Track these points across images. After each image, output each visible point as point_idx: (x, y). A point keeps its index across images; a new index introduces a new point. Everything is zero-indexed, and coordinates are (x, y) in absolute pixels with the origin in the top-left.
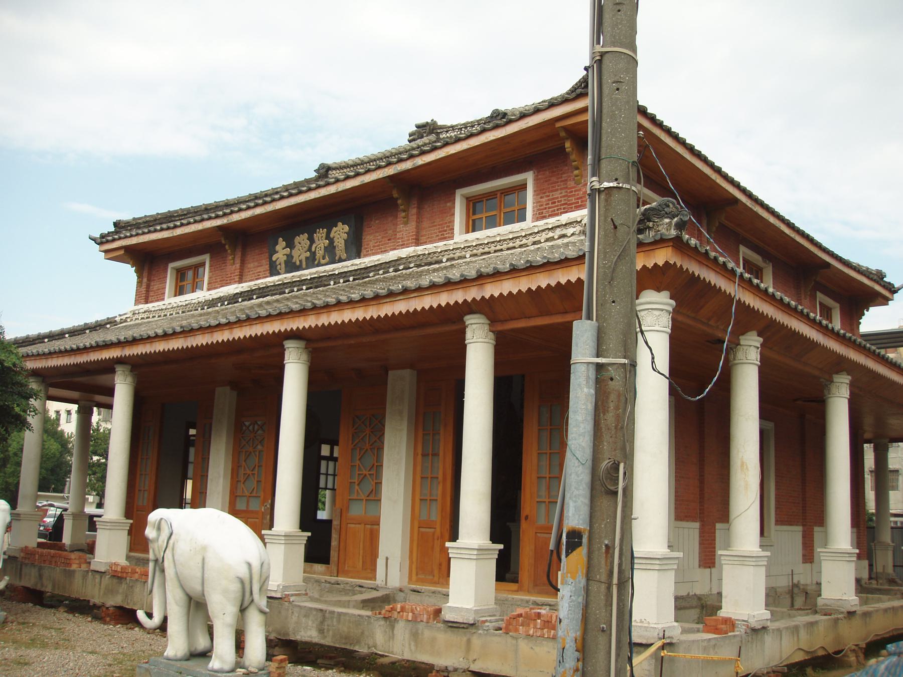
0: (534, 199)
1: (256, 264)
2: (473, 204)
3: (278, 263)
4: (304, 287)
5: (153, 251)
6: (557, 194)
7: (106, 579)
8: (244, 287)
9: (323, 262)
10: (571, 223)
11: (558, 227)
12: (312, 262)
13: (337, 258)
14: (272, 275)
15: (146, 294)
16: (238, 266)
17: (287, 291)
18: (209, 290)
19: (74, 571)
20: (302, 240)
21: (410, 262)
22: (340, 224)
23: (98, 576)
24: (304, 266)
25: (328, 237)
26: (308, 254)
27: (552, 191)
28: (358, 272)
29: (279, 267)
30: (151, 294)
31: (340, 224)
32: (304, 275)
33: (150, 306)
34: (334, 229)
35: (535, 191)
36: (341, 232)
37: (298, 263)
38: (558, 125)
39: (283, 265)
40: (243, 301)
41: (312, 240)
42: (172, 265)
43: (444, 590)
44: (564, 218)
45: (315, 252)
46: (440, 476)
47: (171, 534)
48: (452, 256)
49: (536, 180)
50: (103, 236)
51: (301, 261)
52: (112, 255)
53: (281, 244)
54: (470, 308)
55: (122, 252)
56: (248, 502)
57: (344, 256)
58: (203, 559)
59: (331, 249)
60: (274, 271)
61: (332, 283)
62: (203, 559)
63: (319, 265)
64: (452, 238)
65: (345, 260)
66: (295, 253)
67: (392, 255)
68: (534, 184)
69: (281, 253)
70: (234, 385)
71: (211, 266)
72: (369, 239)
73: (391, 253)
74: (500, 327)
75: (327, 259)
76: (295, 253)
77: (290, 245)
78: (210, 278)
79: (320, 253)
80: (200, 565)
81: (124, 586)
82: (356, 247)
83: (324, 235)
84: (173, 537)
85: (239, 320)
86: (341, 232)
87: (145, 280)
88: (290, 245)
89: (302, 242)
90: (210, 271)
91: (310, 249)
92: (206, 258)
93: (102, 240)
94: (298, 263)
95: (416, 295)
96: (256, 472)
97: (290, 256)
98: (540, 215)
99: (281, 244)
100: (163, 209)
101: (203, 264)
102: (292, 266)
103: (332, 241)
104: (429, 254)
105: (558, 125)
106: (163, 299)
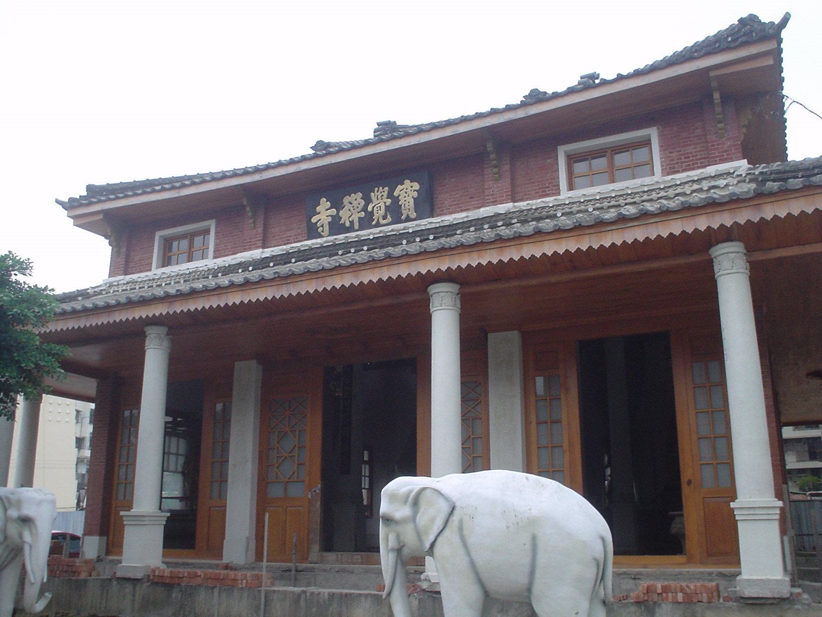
0: (661, 154)
1: (284, 228)
2: (572, 159)
3: (319, 224)
4: (365, 248)
5: (131, 219)
6: (690, 149)
7: (142, 590)
8: (268, 252)
9: (382, 222)
10: (720, 175)
11: (704, 179)
12: (367, 221)
13: (403, 217)
14: (309, 238)
15: (123, 262)
16: (260, 230)
17: (340, 252)
18: (215, 257)
19: (85, 581)
20: (354, 201)
21: (511, 218)
22: (407, 182)
23: (129, 588)
24: (356, 226)
25: (390, 195)
26: (363, 214)
27: (684, 146)
28: (440, 230)
29: (320, 230)
30: (132, 265)
31: (407, 182)
32: (350, 237)
33: (128, 278)
34: (400, 187)
35: (661, 147)
37: (348, 224)
38: (712, 74)
39: (326, 228)
40: (274, 265)
41: (368, 200)
42: (158, 234)
43: (737, 570)
44: (711, 170)
45: (372, 212)
46: (566, 445)
47: (453, 508)
48: (567, 210)
49: (661, 136)
50: (72, 200)
51: (352, 223)
52: (85, 222)
53: (324, 204)
54: (725, 235)
55: (101, 217)
56: (285, 489)
57: (413, 215)
58: (534, 538)
59: (395, 212)
60: (313, 232)
61: (404, 242)
62: (534, 538)
63: (378, 225)
64: (559, 194)
65: (414, 220)
66: (344, 214)
67: (473, 215)
68: (660, 140)
69: (324, 213)
70: (262, 358)
71: (217, 233)
72: (443, 198)
73: (482, 209)
74: (760, 256)
75: (389, 219)
76: (344, 214)
77: (337, 204)
78: (216, 245)
79: (379, 214)
80: (528, 547)
81: (176, 594)
82: (427, 204)
83: (385, 194)
84: (456, 512)
85: (374, 260)
87: (124, 250)
88: (337, 204)
89: (355, 203)
90: (217, 237)
91: (365, 209)
92: (212, 224)
93: (71, 205)
94: (348, 224)
95: (657, 220)
96: (296, 453)
97: (335, 220)
98: (670, 169)
99: (324, 204)
100: (141, 177)
101: (207, 232)
102: (336, 227)
103: (396, 200)
104: (536, 209)
105: (712, 74)
106: (150, 270)
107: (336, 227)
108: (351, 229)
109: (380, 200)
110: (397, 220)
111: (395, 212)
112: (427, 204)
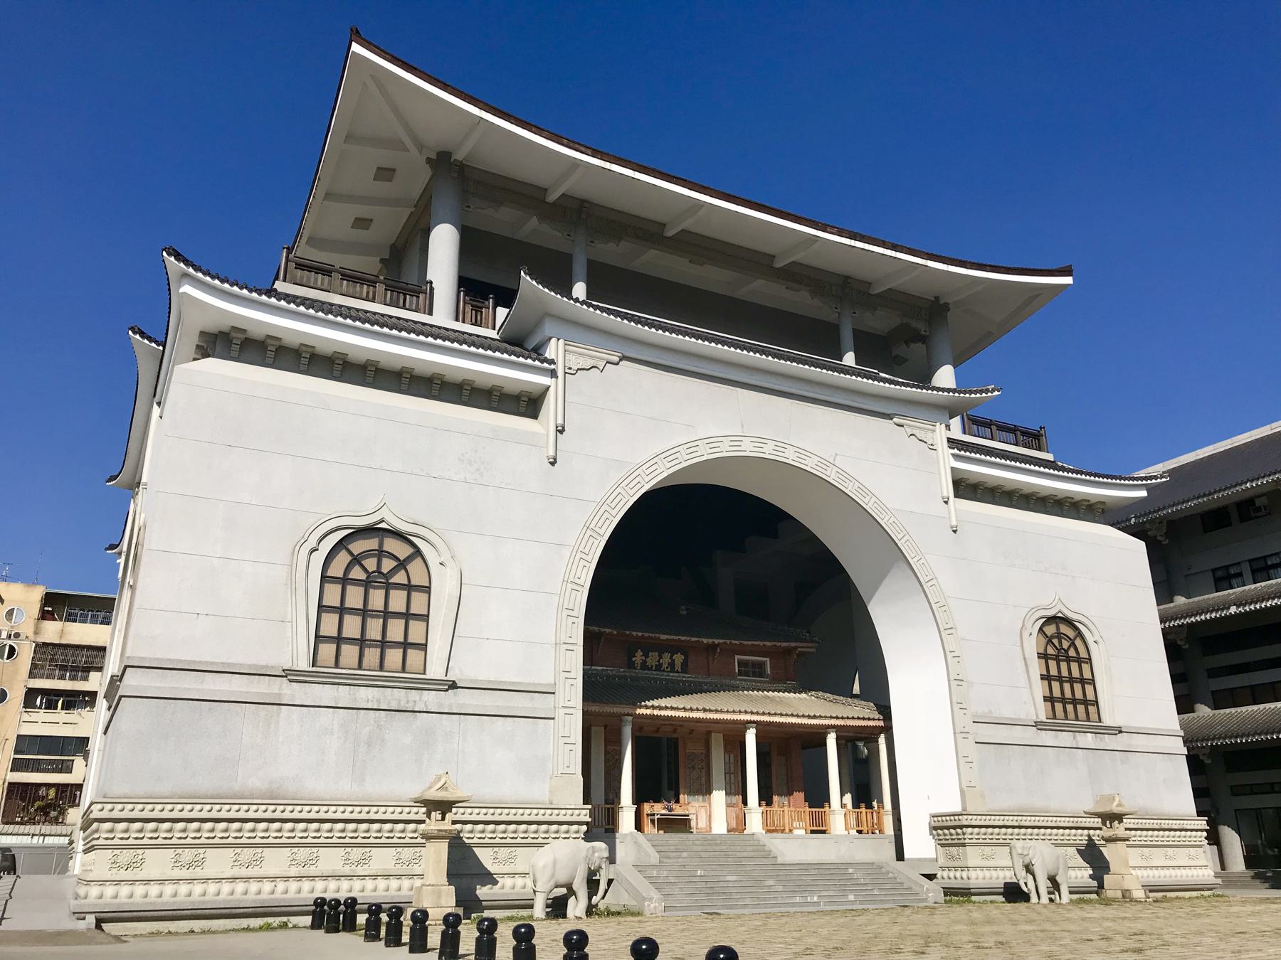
36: (679, 658)
53: (639, 653)
69: (638, 657)
77: (646, 655)
79: (665, 666)
86: (679, 658)
88: (646, 655)
103: (673, 661)
107: (644, 666)
108: (650, 669)
109: (666, 659)
110: (673, 670)
111: (672, 665)
112: (685, 667)
